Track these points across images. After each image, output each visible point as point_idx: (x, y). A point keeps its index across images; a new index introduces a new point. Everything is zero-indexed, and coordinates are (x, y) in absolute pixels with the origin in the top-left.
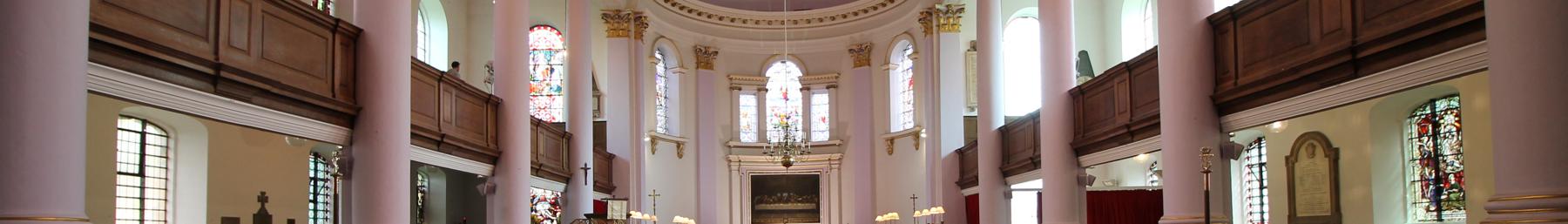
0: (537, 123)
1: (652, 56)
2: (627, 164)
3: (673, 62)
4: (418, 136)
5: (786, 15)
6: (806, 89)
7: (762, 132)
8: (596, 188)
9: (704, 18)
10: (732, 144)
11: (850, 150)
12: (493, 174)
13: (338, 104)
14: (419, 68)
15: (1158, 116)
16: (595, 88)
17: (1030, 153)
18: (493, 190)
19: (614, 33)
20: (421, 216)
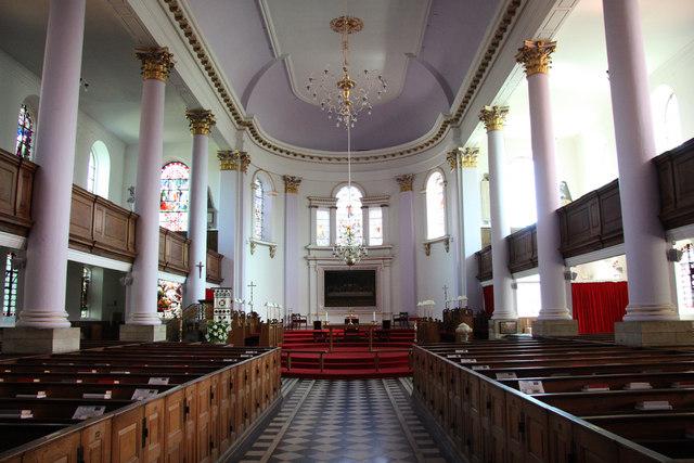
0: (165, 232)
3: (268, 188)
4: (75, 242)
5: (349, 154)
6: (365, 207)
8: (209, 279)
9: (284, 154)
12: (131, 270)
13: (17, 219)
14: (79, 192)
15: (622, 229)
16: (210, 205)
17: (529, 256)
18: (131, 282)
19: (226, 167)
20: (85, 299)
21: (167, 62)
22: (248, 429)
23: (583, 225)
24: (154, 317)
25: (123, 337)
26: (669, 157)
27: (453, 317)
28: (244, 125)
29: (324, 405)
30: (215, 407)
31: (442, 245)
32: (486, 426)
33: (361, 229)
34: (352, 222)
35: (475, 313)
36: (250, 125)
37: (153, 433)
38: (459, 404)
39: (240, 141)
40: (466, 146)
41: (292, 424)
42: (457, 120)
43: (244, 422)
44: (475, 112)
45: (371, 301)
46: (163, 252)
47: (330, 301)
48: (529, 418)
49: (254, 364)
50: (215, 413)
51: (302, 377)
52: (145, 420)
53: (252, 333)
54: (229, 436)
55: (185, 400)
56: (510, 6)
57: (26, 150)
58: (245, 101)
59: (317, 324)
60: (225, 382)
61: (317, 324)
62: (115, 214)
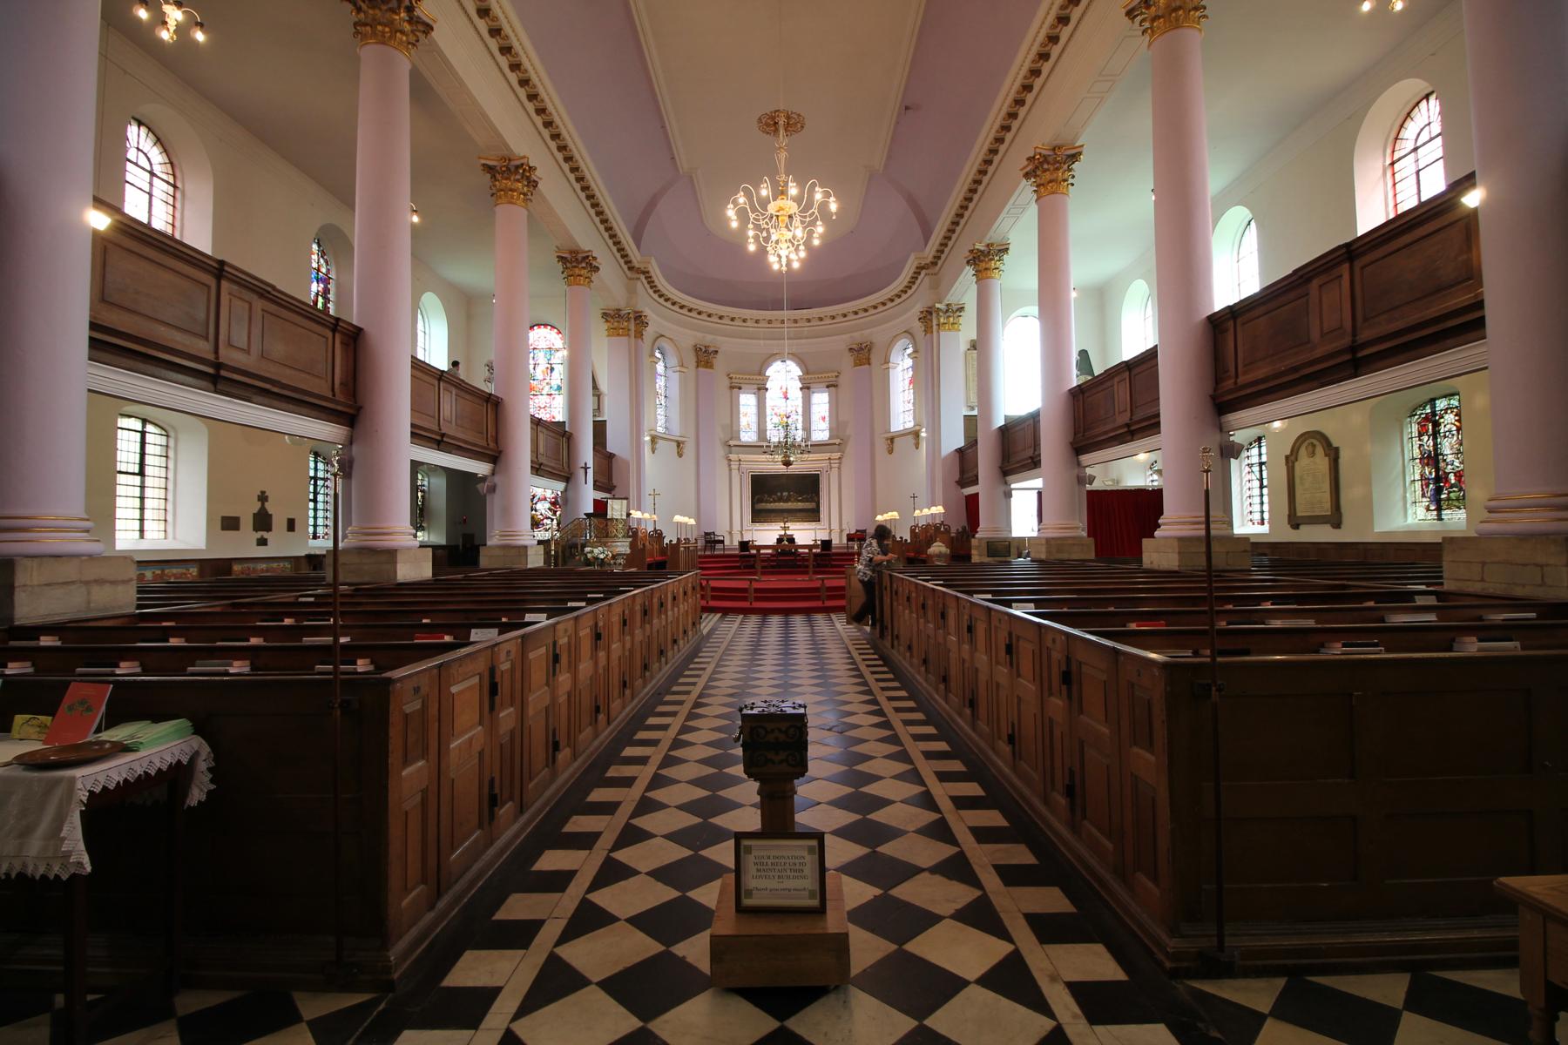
0: (537, 422)
1: (653, 355)
2: (627, 464)
3: (673, 361)
4: (418, 435)
6: (806, 388)
7: (762, 431)
8: (597, 487)
9: (704, 317)
13: (338, 403)
14: (419, 367)
15: (1158, 415)
16: (595, 387)
17: (1030, 453)
18: (493, 489)
19: (614, 332)
20: (422, 515)
21: (528, 178)
22: (602, 737)
23: (1107, 405)
24: (529, 538)
25: (484, 561)
26: (1233, 312)
29: (756, 647)
31: (910, 438)
34: (784, 404)
35: (953, 530)
36: (645, 272)
37: (564, 659)
39: (632, 292)
41: (718, 665)
42: (934, 264)
44: (960, 250)
45: (813, 515)
48: (1018, 638)
50: (628, 645)
51: (725, 612)
53: (655, 558)
57: (325, 305)
58: (637, 239)
60: (638, 608)
61: (744, 545)
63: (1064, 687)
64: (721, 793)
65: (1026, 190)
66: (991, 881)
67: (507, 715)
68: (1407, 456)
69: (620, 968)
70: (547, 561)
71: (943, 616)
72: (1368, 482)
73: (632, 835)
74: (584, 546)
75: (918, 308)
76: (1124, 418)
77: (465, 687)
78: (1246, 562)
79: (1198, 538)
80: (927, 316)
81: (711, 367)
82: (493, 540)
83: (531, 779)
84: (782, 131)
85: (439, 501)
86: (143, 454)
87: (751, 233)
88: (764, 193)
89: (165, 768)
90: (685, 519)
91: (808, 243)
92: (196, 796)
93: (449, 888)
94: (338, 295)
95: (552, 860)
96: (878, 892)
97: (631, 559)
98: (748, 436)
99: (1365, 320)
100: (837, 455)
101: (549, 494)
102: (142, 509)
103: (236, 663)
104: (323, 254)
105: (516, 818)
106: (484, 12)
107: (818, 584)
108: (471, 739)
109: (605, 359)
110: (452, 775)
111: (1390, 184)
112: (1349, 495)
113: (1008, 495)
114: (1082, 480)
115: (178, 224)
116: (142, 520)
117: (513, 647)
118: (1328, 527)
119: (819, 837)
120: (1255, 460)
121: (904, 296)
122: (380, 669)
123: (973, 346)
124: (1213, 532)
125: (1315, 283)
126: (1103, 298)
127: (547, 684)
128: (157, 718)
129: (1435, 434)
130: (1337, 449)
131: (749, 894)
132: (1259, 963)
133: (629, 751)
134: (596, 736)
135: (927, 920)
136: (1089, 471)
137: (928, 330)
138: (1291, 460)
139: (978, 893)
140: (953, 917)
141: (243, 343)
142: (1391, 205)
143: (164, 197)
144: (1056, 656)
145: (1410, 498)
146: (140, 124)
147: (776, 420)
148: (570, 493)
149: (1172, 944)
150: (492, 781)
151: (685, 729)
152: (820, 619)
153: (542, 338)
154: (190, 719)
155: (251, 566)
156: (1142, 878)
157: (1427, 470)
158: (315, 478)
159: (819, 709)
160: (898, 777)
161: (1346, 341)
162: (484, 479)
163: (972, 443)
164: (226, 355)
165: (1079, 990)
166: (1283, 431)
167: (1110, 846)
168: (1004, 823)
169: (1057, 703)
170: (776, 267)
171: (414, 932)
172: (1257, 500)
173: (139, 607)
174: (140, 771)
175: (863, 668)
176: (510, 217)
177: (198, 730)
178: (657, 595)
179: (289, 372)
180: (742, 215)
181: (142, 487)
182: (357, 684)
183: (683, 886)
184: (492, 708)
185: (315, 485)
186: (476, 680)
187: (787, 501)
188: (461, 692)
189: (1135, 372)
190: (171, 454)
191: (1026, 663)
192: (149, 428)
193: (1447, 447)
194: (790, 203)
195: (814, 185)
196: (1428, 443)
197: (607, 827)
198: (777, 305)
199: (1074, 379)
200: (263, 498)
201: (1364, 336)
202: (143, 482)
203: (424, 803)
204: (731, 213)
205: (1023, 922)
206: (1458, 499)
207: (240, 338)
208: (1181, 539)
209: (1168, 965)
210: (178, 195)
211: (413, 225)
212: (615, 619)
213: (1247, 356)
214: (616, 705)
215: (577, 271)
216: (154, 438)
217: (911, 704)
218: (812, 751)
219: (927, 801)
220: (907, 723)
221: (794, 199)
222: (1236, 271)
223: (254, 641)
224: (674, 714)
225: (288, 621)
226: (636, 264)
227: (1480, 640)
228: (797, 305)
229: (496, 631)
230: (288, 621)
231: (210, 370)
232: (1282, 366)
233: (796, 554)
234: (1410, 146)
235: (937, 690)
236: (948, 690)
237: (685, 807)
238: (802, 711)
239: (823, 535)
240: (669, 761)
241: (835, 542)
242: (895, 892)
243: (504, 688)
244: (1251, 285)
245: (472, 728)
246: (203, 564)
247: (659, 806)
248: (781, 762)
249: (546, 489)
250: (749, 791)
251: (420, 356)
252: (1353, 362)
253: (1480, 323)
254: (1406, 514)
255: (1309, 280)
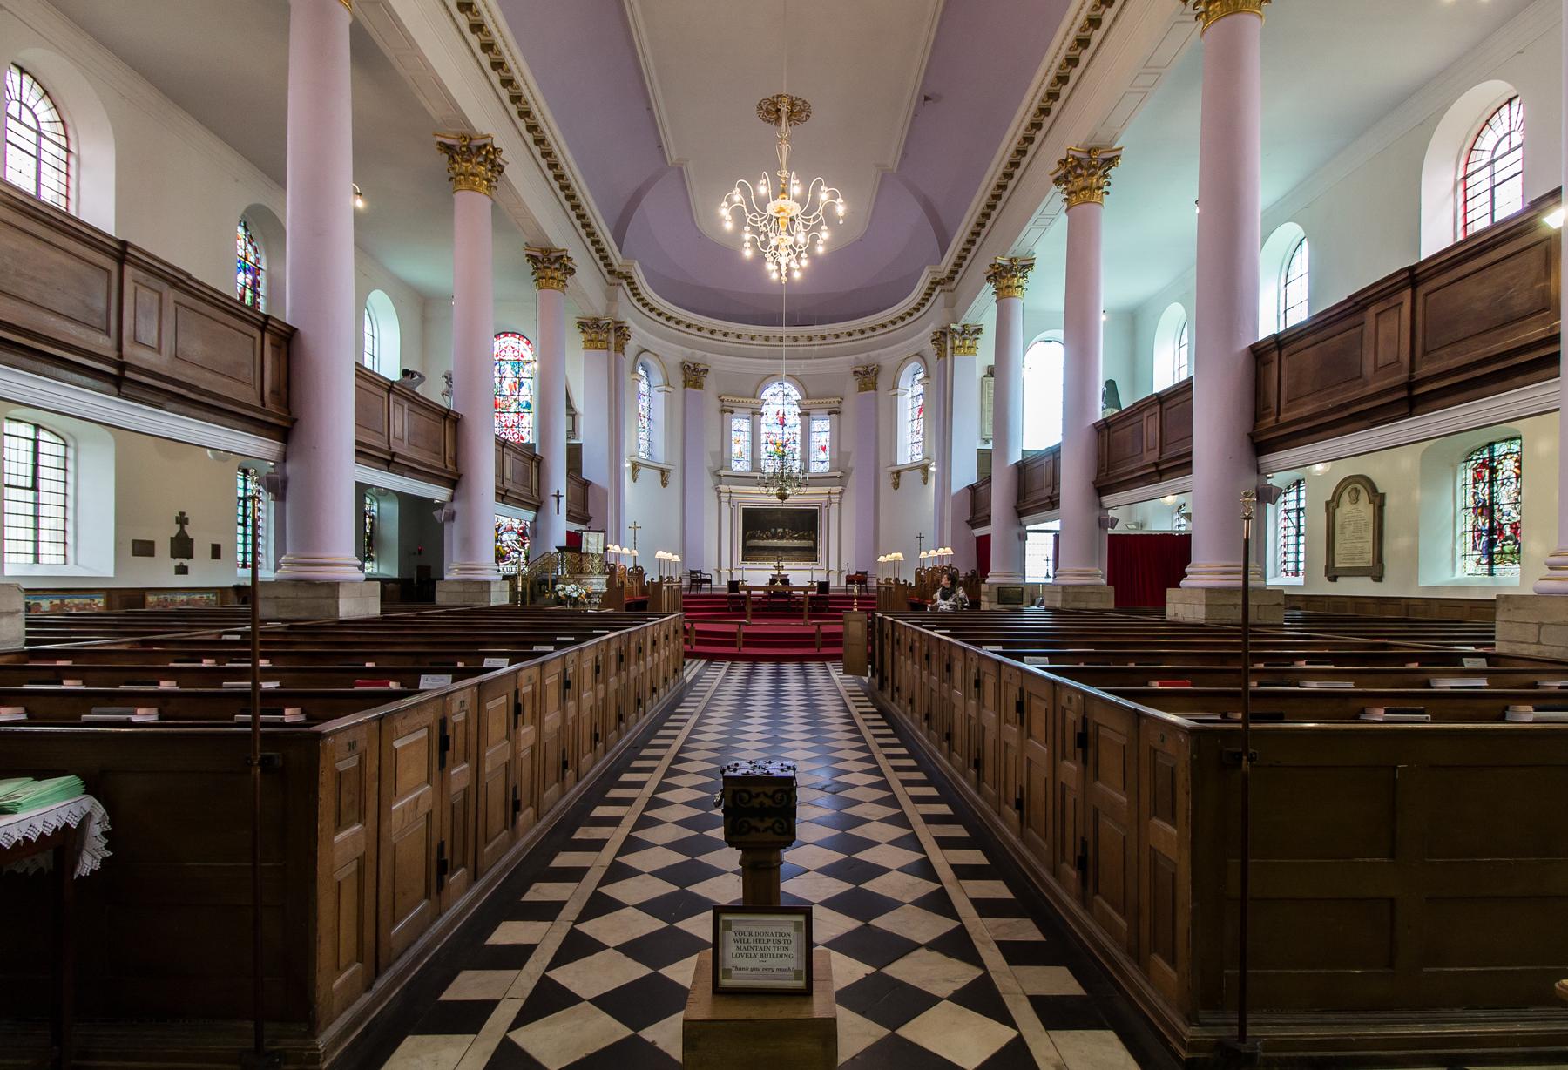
0: (502, 444)
1: (634, 371)
3: (658, 379)
4: (364, 453)
6: (805, 414)
7: (755, 461)
10: (722, 472)
11: (852, 482)
12: (452, 499)
14: (362, 373)
15: (1190, 454)
16: (569, 406)
17: (1048, 492)
18: (451, 517)
19: (591, 344)
20: (370, 544)
21: (492, 162)
24: (490, 571)
25: (441, 598)
26: (1279, 342)
27: (928, 582)
28: (615, 275)
29: (744, 696)
30: (601, 686)
32: (972, 712)
33: (798, 448)
34: (780, 429)
36: (628, 278)
37: (527, 710)
38: (936, 687)
39: (611, 299)
40: (962, 322)
41: (702, 716)
42: (951, 279)
43: (636, 711)
44: (980, 265)
45: (810, 554)
46: (500, 474)
47: (750, 553)
48: (1030, 694)
49: (650, 631)
50: (601, 695)
51: (711, 658)
52: (517, 692)
53: (635, 600)
54: (618, 728)
55: (565, 671)
56: (1061, 67)
57: (254, 300)
58: (619, 238)
59: (733, 586)
60: (613, 653)
61: (733, 586)
62: (422, 411)
63: (1079, 750)
64: (700, 858)
65: (1055, 198)
66: (994, 959)
67: (460, 772)
68: (1460, 505)
69: (582, 1055)
70: (513, 598)
71: (949, 668)
72: (1415, 535)
73: (600, 905)
74: (555, 582)
75: (931, 328)
76: (1152, 457)
77: (410, 742)
78: (1279, 617)
79: (1230, 591)
80: (941, 337)
81: (701, 387)
82: (452, 574)
83: (487, 842)
84: (784, 119)
85: (391, 529)
86: (36, 466)
87: (747, 236)
88: (763, 190)
89: (49, 832)
90: (669, 556)
91: (810, 250)
92: (88, 863)
93: (390, 965)
94: (269, 288)
95: (507, 934)
96: (870, 970)
97: (607, 599)
98: (741, 466)
99: (1425, 353)
100: (838, 489)
101: (516, 524)
102: (37, 529)
103: (140, 711)
104: (251, 240)
105: (468, 889)
106: (466, 7)
107: (813, 630)
108: (417, 799)
109: (581, 373)
110: (394, 840)
111: (1461, 201)
112: (1395, 544)
113: (1023, 538)
114: (1104, 523)
115: (72, 196)
116: (36, 542)
117: (468, 696)
118: (1368, 580)
119: (805, 910)
120: (1292, 505)
121: (916, 315)
122: (312, 719)
123: (991, 372)
124: (1251, 583)
125: (1372, 310)
126: (1135, 323)
127: (508, 737)
128: (40, 774)
129: (1492, 482)
130: (1383, 496)
131: (728, 972)
132: (1284, 1054)
133: (600, 811)
134: (563, 794)
135: (924, 1001)
136: (1111, 513)
137: (941, 353)
138: (1332, 507)
139: (980, 972)
140: (950, 998)
141: (152, 339)
142: (1460, 224)
143: (55, 162)
144: (1071, 716)
145: (1459, 551)
146: (22, 71)
147: (771, 448)
148: (540, 524)
149: (1190, 1033)
150: (442, 844)
151: (663, 787)
152: (814, 668)
153: (508, 346)
154: (78, 775)
155: (169, 597)
156: (1157, 959)
157: (1481, 520)
158: (245, 499)
159: (812, 766)
160: (894, 843)
161: (1402, 376)
162: (441, 505)
163: (985, 479)
164: (132, 354)
165: (1038, 1003)
166: (1326, 475)
167: (1124, 924)
168: (1009, 895)
169: (1070, 768)
170: (775, 276)
171: (347, 1016)
172: (1292, 549)
173: (28, 642)
174: (17, 836)
175: (859, 722)
176: (472, 206)
177: (90, 789)
178: (614, 646)
179: (208, 375)
180: (738, 214)
181: (36, 504)
182: (283, 739)
183: (656, 961)
184: (442, 764)
185: (245, 507)
186: (424, 733)
187: (782, 537)
188: (405, 747)
189: (1166, 405)
190: (70, 466)
191: (1038, 724)
192: (43, 435)
193: (1504, 496)
194: (792, 203)
195: (819, 184)
196: (1483, 491)
197: (572, 895)
198: (773, 320)
199: (1100, 411)
200: (182, 520)
201: (1424, 370)
202: (37, 498)
203: (360, 870)
204: (724, 212)
205: (1027, 1005)
206: (1512, 553)
207: (148, 333)
208: (1209, 590)
209: (1184, 1055)
210: (72, 161)
211: (356, 211)
212: (587, 666)
213: (1301, 390)
214: (586, 760)
215: (549, 273)
216: (49, 446)
217: (911, 763)
218: (802, 812)
219: (925, 869)
220: (905, 783)
221: (797, 200)
222: (1282, 299)
223: (165, 685)
224: (651, 770)
225: (207, 663)
226: (617, 268)
227: (1536, 710)
228: (792, 322)
229: (449, 678)
230: (207, 663)
231: (113, 371)
232: (1330, 403)
233: (790, 596)
234: (1486, 157)
235: (940, 750)
236: (951, 748)
237: (673, 846)
238: (791, 773)
239: (820, 576)
240: (644, 822)
241: (833, 583)
242: (887, 970)
243: (457, 741)
244: (1299, 315)
245: (417, 787)
246: (109, 593)
247: (631, 872)
248: (766, 829)
249: (513, 519)
250: (730, 858)
251: (368, 364)
252: (1411, 399)
253: (1554, 359)
254: (1449, 566)
255: (1365, 308)
